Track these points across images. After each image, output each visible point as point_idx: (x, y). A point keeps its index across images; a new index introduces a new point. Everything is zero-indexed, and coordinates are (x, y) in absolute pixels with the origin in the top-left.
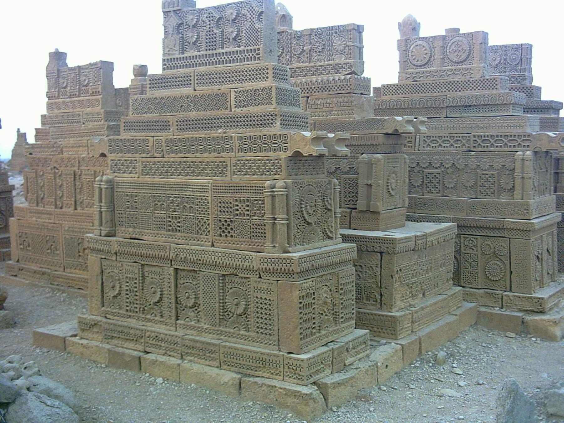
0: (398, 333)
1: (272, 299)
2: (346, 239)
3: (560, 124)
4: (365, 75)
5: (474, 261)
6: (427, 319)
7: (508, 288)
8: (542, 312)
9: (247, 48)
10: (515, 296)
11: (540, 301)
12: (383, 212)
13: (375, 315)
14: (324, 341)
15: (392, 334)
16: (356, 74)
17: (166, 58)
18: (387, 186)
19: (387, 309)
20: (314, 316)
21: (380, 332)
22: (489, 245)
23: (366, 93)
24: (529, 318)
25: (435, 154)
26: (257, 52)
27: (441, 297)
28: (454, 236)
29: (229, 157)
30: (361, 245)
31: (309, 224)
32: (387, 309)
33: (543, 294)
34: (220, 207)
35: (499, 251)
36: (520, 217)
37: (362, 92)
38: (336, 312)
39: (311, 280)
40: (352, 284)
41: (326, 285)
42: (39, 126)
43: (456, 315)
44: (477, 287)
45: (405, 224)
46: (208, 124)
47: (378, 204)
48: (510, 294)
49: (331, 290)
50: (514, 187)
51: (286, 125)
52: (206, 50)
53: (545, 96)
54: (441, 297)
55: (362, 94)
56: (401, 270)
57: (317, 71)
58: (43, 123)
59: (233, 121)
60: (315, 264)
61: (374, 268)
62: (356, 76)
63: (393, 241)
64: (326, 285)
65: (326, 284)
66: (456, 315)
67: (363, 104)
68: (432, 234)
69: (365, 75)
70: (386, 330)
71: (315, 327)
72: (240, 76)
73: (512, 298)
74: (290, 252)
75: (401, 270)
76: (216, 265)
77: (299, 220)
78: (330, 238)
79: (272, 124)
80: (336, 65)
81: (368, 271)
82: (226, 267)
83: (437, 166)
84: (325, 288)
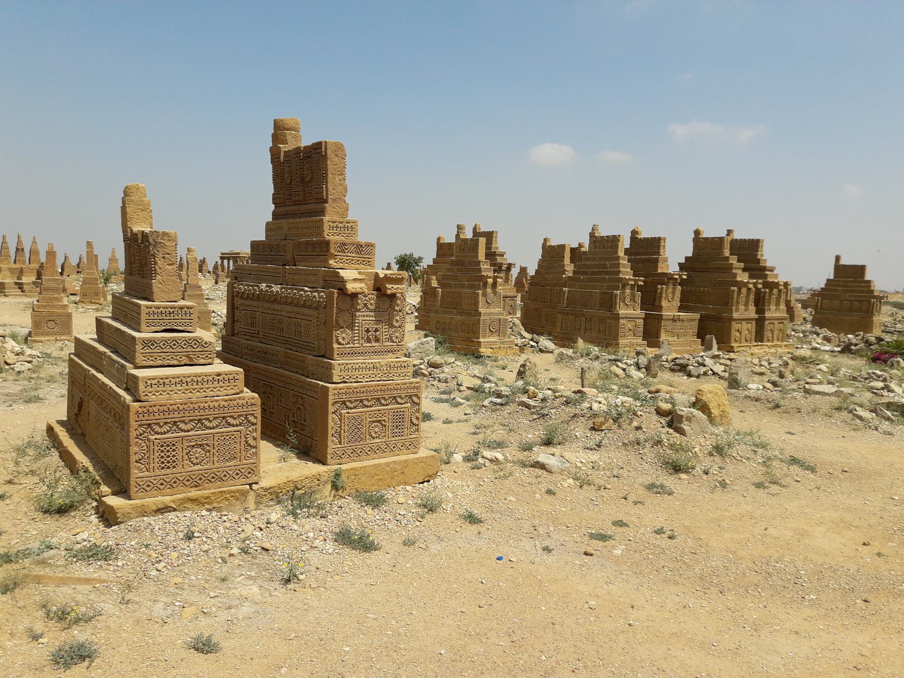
50: (541, 351)
59: (607, 273)
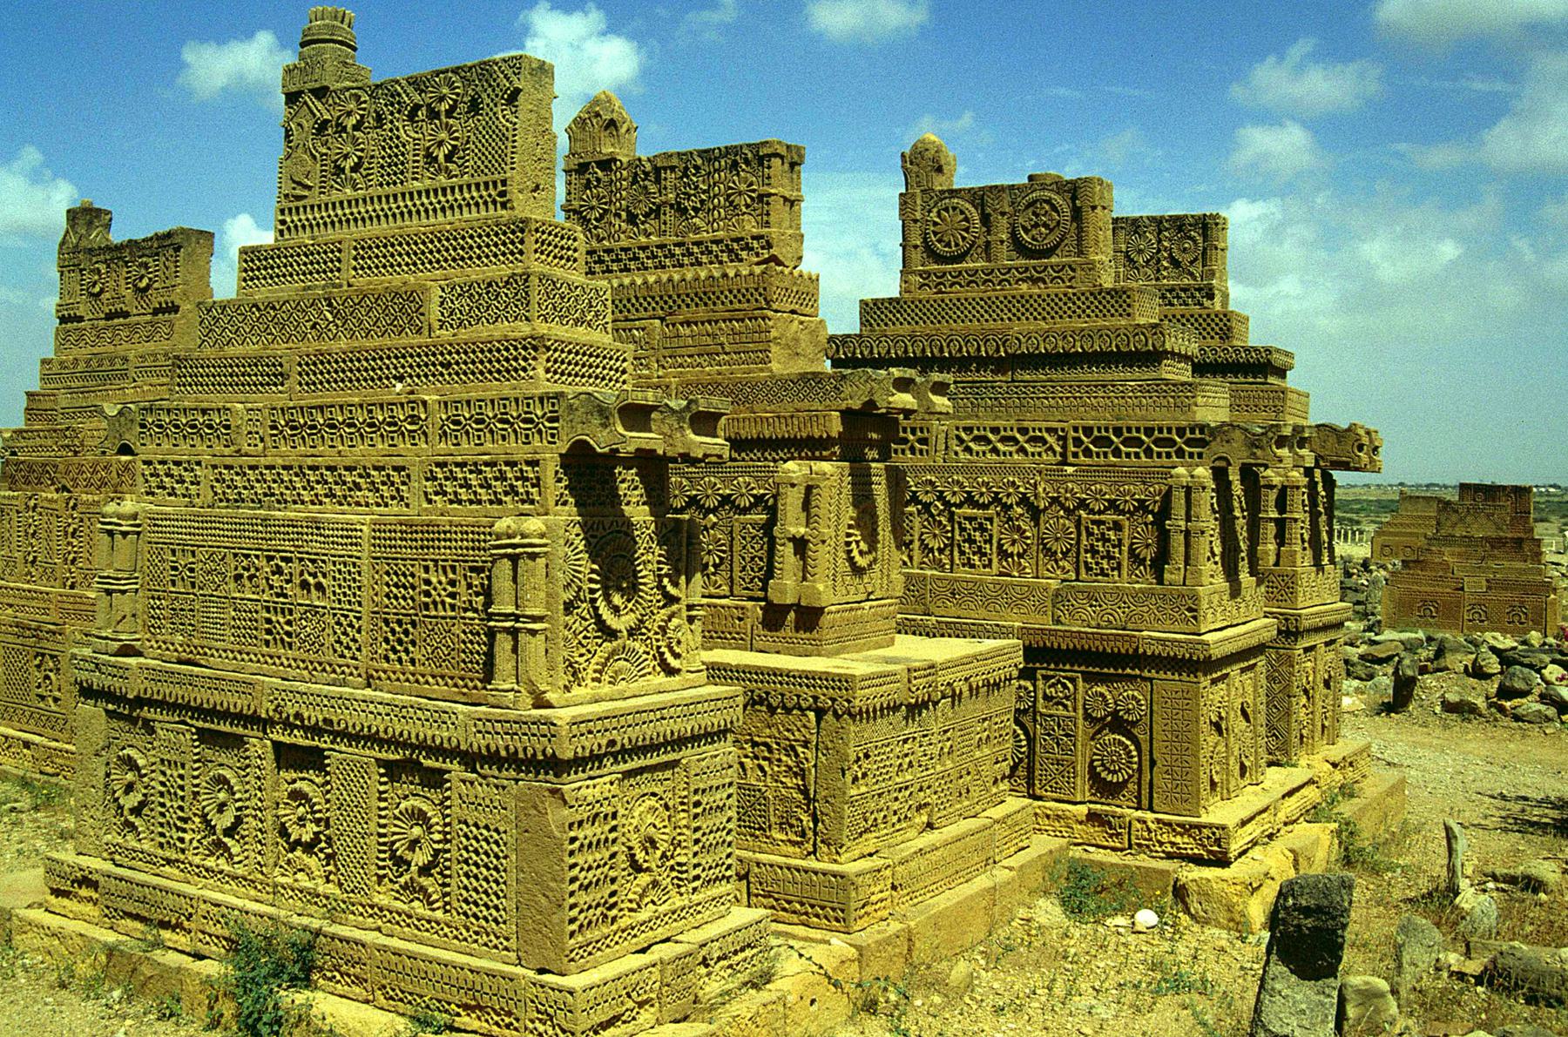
0: (854, 914)
1: (502, 829)
2: (716, 672)
3: (1289, 403)
4: (805, 267)
5: (1067, 735)
6: (933, 879)
7: (1145, 802)
8: (1222, 861)
9: (478, 179)
10: (1159, 821)
11: (1219, 834)
12: (833, 608)
13: (816, 873)
14: (642, 940)
15: (837, 920)
16: (779, 263)
17: (286, 204)
18: (848, 544)
19: (830, 854)
20: (612, 874)
21: (806, 914)
22: (1102, 695)
23: (808, 310)
24: (1191, 874)
25: (982, 471)
26: (500, 188)
27: (973, 824)
28: (1015, 673)
29: (416, 454)
30: (767, 693)
31: (611, 634)
32: (830, 854)
33: (1218, 812)
34: (388, 585)
35: (1128, 711)
36: (1177, 627)
37: (793, 307)
38: (679, 864)
39: (607, 779)
40: (731, 791)
41: (654, 794)
42: (36, 387)
43: (1011, 869)
44: (1071, 798)
45: (893, 640)
46: (371, 367)
47: (821, 587)
48: (1149, 816)
49: (667, 807)
51: (562, 374)
52: (381, 185)
53: (1255, 337)
54: (973, 824)
55: (793, 312)
56: (867, 756)
57: (692, 253)
58: (45, 378)
59: (441, 363)
60: (618, 739)
61: (800, 749)
62: (779, 268)
63: (844, 682)
64: (654, 794)
65: (656, 790)
66: (1011, 869)
67: (796, 340)
68: (949, 665)
69: (805, 267)
70: (823, 908)
71: (615, 904)
72: (455, 249)
73: (1153, 826)
74: (551, 706)
75: (867, 756)
76: (373, 739)
77: (585, 624)
78: (671, 672)
79: (524, 370)
80: (733, 240)
81: (784, 758)
82: (394, 742)
83: (985, 499)
84: (652, 802)
